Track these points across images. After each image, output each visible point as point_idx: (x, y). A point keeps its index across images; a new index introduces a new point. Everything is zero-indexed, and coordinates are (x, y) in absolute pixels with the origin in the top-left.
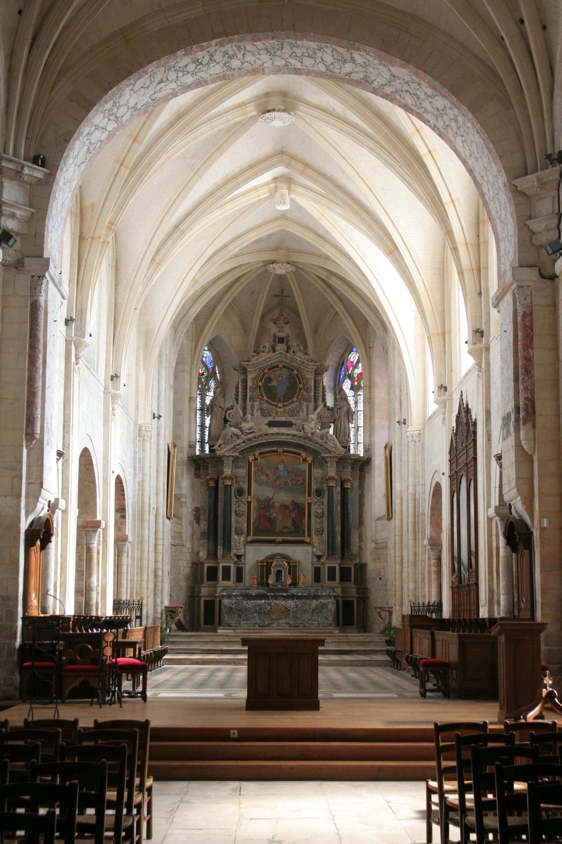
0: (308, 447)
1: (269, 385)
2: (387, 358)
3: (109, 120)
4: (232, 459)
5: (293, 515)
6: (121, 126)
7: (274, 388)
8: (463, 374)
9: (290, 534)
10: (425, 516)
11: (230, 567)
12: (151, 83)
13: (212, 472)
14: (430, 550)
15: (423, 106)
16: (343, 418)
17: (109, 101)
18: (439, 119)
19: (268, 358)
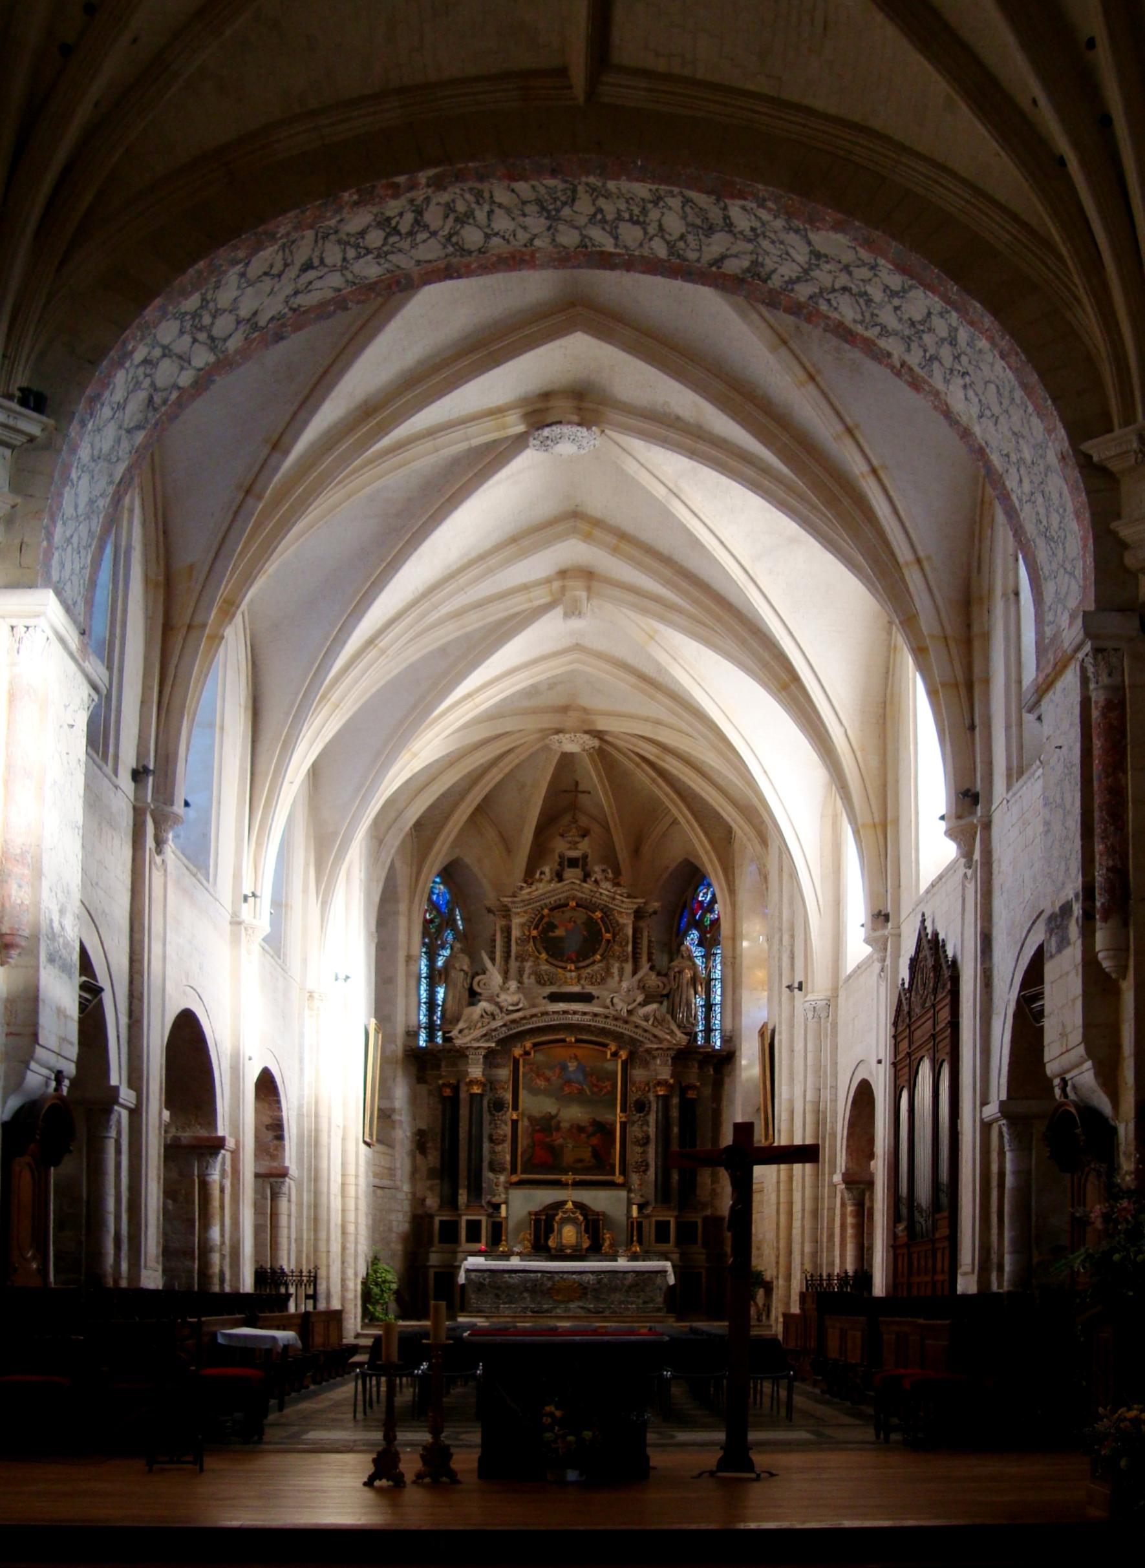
0: (622, 1033)
1: (551, 934)
2: (767, 888)
3: (195, 340)
4: (483, 1052)
5: (594, 1141)
6: (225, 364)
7: (560, 939)
8: (924, 885)
9: (587, 1170)
10: (836, 1137)
11: (479, 1222)
12: (286, 265)
13: (446, 1074)
14: (845, 1191)
15: (879, 320)
16: (685, 988)
17: (191, 293)
18: (914, 346)
19: (550, 892)
